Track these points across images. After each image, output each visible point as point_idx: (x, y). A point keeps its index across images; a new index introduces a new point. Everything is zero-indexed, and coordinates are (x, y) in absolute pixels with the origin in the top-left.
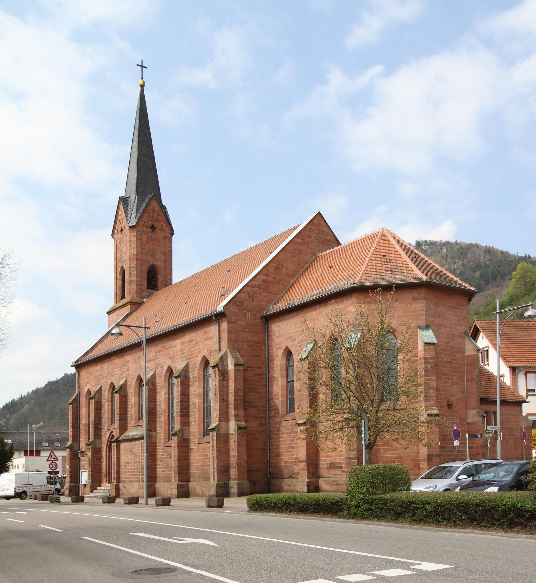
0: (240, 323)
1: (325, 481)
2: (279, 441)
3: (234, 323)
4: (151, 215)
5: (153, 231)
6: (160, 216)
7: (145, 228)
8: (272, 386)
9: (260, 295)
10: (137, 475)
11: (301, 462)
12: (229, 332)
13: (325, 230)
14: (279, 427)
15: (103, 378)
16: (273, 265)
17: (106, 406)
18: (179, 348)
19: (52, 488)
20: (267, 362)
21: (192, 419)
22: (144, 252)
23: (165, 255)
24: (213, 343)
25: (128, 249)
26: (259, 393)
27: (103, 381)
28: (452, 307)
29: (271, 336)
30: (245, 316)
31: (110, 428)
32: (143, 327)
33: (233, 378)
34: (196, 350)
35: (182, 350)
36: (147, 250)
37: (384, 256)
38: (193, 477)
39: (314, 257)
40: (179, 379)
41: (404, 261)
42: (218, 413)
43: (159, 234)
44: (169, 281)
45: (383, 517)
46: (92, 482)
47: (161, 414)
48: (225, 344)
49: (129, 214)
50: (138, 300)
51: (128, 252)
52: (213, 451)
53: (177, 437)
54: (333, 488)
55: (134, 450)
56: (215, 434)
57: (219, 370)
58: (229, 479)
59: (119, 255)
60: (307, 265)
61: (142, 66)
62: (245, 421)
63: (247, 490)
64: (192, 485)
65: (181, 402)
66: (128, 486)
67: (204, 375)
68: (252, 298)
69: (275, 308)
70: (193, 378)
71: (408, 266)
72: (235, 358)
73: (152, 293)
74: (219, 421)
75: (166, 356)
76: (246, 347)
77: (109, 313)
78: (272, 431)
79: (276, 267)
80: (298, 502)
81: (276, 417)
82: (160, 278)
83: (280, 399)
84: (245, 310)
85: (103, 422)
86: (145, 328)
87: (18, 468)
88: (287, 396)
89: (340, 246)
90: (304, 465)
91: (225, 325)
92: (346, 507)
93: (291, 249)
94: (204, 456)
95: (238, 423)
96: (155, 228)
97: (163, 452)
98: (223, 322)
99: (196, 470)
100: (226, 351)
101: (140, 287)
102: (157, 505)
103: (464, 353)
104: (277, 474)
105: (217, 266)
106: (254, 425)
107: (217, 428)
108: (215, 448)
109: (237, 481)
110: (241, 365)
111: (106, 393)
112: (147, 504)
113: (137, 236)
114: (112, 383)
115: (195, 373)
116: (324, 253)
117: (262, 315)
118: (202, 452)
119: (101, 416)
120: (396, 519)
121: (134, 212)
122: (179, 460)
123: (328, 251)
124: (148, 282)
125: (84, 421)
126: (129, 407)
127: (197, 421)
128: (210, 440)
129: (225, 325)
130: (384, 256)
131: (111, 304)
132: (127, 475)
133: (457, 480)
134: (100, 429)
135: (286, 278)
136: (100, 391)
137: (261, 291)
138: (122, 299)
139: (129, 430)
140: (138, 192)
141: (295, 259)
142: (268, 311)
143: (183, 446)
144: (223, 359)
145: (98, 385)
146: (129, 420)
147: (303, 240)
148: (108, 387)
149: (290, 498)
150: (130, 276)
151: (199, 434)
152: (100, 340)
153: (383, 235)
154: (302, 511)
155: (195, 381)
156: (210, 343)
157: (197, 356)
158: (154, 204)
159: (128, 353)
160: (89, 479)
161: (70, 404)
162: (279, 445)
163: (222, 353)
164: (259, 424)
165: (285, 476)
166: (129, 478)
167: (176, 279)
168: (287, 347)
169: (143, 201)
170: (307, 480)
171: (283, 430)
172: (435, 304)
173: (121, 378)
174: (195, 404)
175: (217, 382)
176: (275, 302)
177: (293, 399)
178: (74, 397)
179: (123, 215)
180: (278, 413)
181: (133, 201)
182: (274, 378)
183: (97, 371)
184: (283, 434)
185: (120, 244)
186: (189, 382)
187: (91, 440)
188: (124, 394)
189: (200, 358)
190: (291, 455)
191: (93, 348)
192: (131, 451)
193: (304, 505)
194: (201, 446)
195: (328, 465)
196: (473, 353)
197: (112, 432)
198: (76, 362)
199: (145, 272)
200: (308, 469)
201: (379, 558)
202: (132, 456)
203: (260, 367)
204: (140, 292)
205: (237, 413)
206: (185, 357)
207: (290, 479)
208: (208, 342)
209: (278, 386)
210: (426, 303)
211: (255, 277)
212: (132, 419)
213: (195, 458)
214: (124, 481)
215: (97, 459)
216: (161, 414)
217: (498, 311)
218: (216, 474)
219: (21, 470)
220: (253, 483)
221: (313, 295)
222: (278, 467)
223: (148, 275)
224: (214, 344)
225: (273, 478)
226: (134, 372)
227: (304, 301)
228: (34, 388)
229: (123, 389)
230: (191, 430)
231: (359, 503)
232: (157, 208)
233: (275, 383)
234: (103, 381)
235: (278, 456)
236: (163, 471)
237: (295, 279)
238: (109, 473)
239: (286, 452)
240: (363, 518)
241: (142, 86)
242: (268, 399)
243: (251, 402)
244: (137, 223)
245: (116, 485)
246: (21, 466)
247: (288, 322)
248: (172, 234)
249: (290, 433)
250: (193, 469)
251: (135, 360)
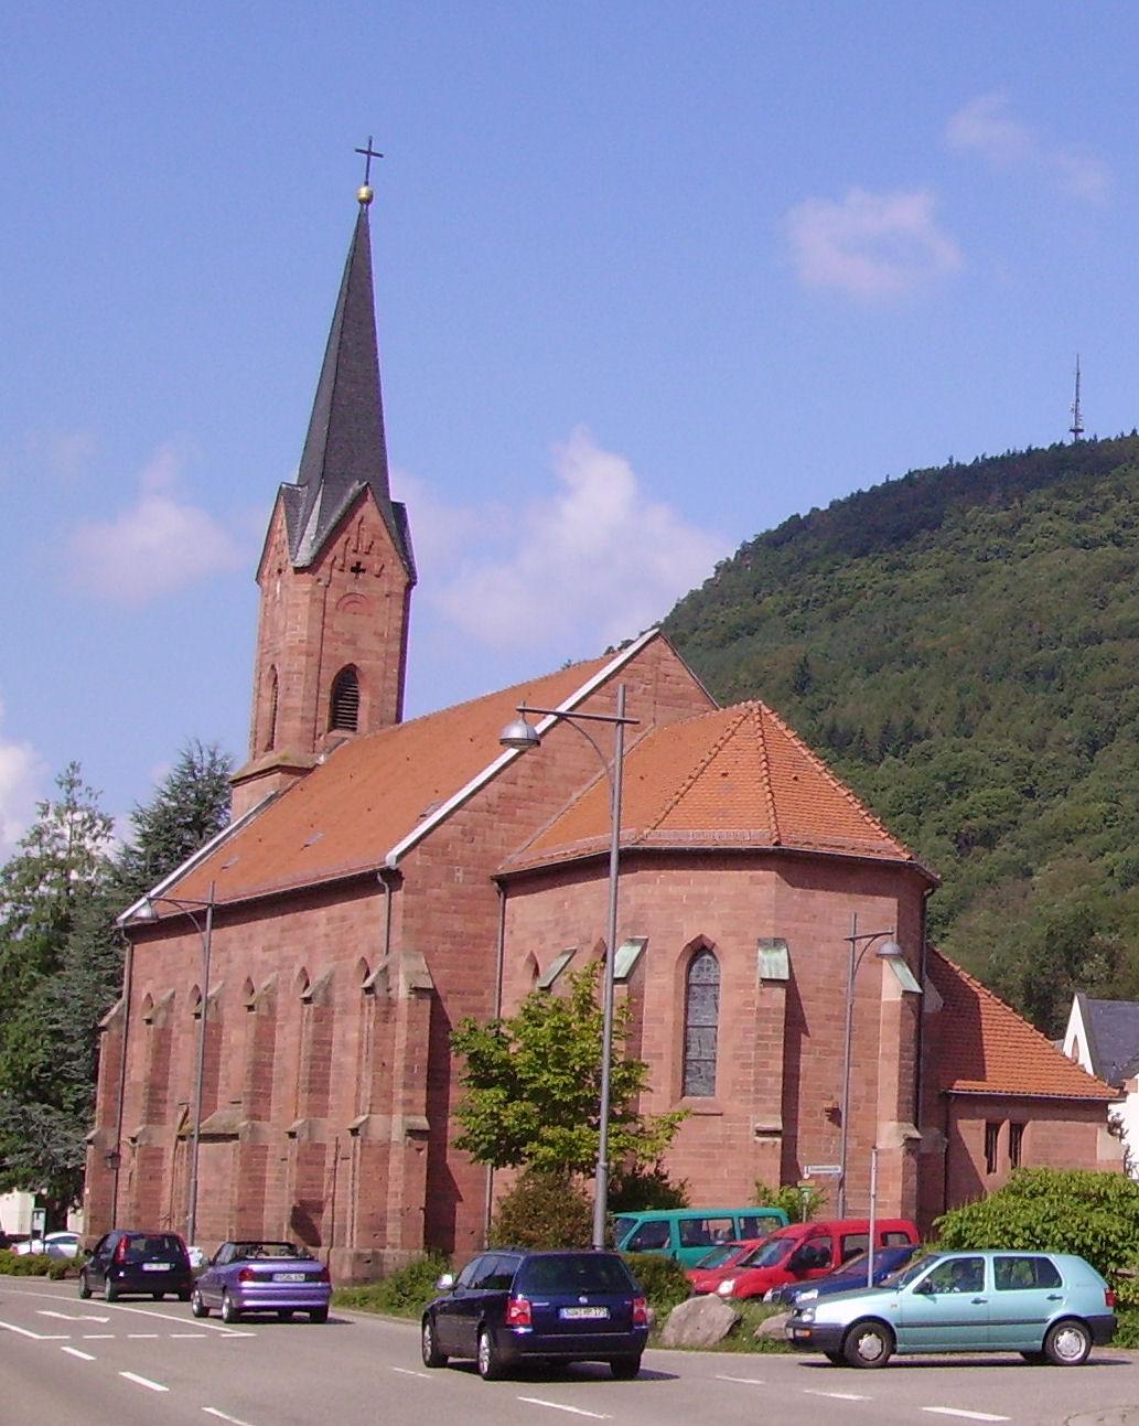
3: (421, 892)
9: (491, 828)
18: (322, 930)
30: (450, 876)
35: (327, 936)
52: (353, 1179)
57: (376, 998)
61: (369, 153)
68: (468, 835)
76: (448, 946)
84: (451, 862)
117: (492, 873)
137: (495, 817)
143: (309, 1163)
145: (169, 987)
157: (351, 956)
166: (209, 1229)
189: (356, 961)
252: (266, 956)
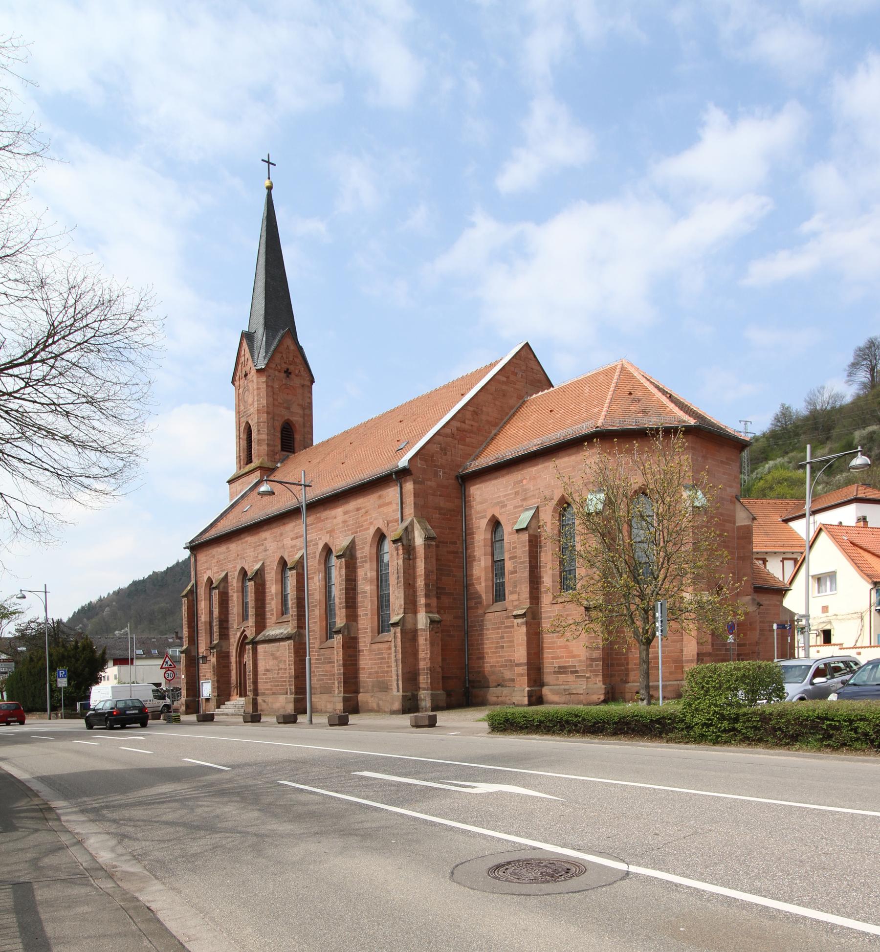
0: (429, 483)
1: (551, 690)
2: (482, 640)
4: (284, 356)
5: (288, 376)
6: (296, 357)
7: (277, 373)
8: (472, 567)
9: (455, 447)
10: (282, 685)
11: (518, 665)
12: (416, 495)
13: (534, 367)
14: (482, 621)
15: (229, 562)
16: (470, 408)
17: (235, 598)
19: (162, 703)
20: (465, 536)
21: (360, 612)
22: (276, 403)
23: (304, 409)
24: (393, 511)
25: (256, 398)
26: (454, 576)
27: (230, 566)
28: (722, 462)
29: (470, 501)
30: (436, 474)
31: (240, 627)
32: (301, 485)
33: (423, 556)
34: (366, 520)
35: (345, 522)
36: (280, 401)
37: (630, 394)
38: (364, 687)
39: (521, 401)
40: (343, 560)
41: (658, 400)
42: (402, 603)
43: (296, 382)
44: (309, 442)
45: (760, 740)
46: (218, 696)
47: (315, 606)
48: (409, 510)
49: (256, 357)
50: (269, 465)
51: (256, 403)
53: (341, 635)
54: (563, 699)
55: (278, 654)
56: (398, 629)
57: (403, 545)
58: (418, 688)
59: (242, 408)
60: (512, 411)
62: (438, 613)
63: (442, 704)
64: (361, 697)
65: (347, 589)
66: (270, 699)
67: (377, 553)
68: (444, 451)
69: (475, 465)
70: (362, 558)
71: (666, 407)
72: (425, 529)
73: (288, 456)
74: (405, 612)
75: (321, 530)
76: (437, 516)
77: (230, 482)
78: (472, 627)
79: (474, 411)
80: (584, 720)
81: (477, 608)
82: (298, 437)
83: (483, 584)
85: (230, 619)
86: (305, 486)
87: (108, 679)
88: (492, 580)
89: (552, 389)
90: (523, 670)
91: (409, 486)
92: (682, 725)
93: (492, 388)
94: (381, 660)
95: (430, 615)
96: (290, 373)
97: (318, 655)
98: (406, 481)
99: (368, 677)
100: (412, 521)
101: (272, 448)
102: (331, 725)
103: (734, 523)
104: (480, 682)
105: (380, 418)
106: (448, 618)
107: (401, 623)
108: (399, 649)
109: (429, 692)
110: (433, 539)
111: (235, 581)
112: (311, 723)
113: (267, 382)
114: (243, 568)
115: (365, 551)
116: (534, 396)
117: (457, 474)
118: (376, 655)
119: (228, 611)
120: (787, 744)
121: (263, 351)
122: (344, 665)
123: (540, 393)
124: (282, 442)
125: (203, 618)
126: (268, 598)
127: (369, 614)
128: (391, 638)
129: (409, 486)
130: (630, 394)
131: (232, 469)
132: (268, 686)
133: (812, 684)
134: (227, 628)
135: (487, 427)
136: (225, 579)
137: (456, 442)
138: (247, 464)
139: (268, 628)
140: (267, 326)
141: (497, 403)
142: (465, 469)
143: (349, 647)
144: (408, 530)
145: (222, 571)
146: (268, 615)
147: (508, 377)
148: (237, 573)
149: (568, 714)
150: (258, 434)
151: (372, 631)
152: (222, 515)
153: (623, 369)
154: (590, 733)
155: (366, 562)
156: (389, 510)
157: (368, 529)
158: (289, 342)
159: (265, 528)
160: (213, 692)
161: (183, 597)
162: (483, 644)
163: (406, 524)
164: (455, 618)
165: (491, 685)
167: (316, 441)
168: (493, 516)
169: (274, 338)
170: (527, 689)
171: (488, 625)
172: (703, 457)
173: (256, 561)
174: (366, 592)
175: (401, 562)
176: (472, 457)
177: (503, 584)
178: (189, 588)
179: (248, 355)
180: (481, 603)
181: (260, 337)
182: (474, 557)
183: (221, 554)
184: (488, 629)
185: (244, 392)
186: (356, 563)
187: (215, 642)
188: (260, 582)
189: (372, 531)
190: (501, 657)
191: (212, 525)
192: (272, 655)
193: (595, 723)
194: (375, 646)
195: (557, 669)
196: (747, 523)
197: (244, 631)
198: (190, 543)
199: (279, 429)
200: (528, 675)
201: (695, 795)
202: (274, 663)
203: (455, 543)
204: (271, 454)
205: (429, 602)
206: (349, 530)
207: (499, 688)
208: (385, 510)
209: (481, 569)
210: (693, 454)
211: (448, 423)
212: (272, 614)
213: (367, 662)
214: (264, 694)
215: (224, 667)
216: (315, 606)
217: (808, 460)
218: (400, 683)
219: (113, 682)
220: (449, 694)
221: (534, 444)
222: (481, 673)
223: (282, 433)
224: (393, 511)
225: (473, 687)
226: (273, 552)
227: (521, 453)
228: (116, 589)
229: (259, 575)
230: (360, 626)
231: (712, 720)
232: (292, 347)
233: (475, 563)
234: (230, 566)
235: (481, 657)
236: (318, 680)
237: (498, 428)
238: (240, 684)
239: (493, 653)
240: (716, 742)
241: (269, 188)
242: (466, 584)
243: (444, 588)
244: (267, 365)
245: (253, 699)
246: (112, 678)
247: (494, 482)
248: (312, 381)
249: (498, 628)
250: (364, 677)
251: (275, 537)
252: (294, 542)
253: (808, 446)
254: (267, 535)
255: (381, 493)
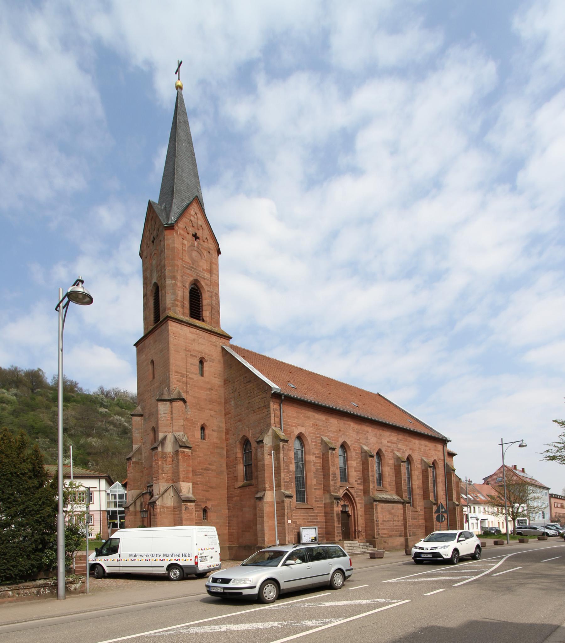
55: (393, 511)
252: (389, 444)
253: (71, 447)
254: (334, 422)
255: (329, 418)
